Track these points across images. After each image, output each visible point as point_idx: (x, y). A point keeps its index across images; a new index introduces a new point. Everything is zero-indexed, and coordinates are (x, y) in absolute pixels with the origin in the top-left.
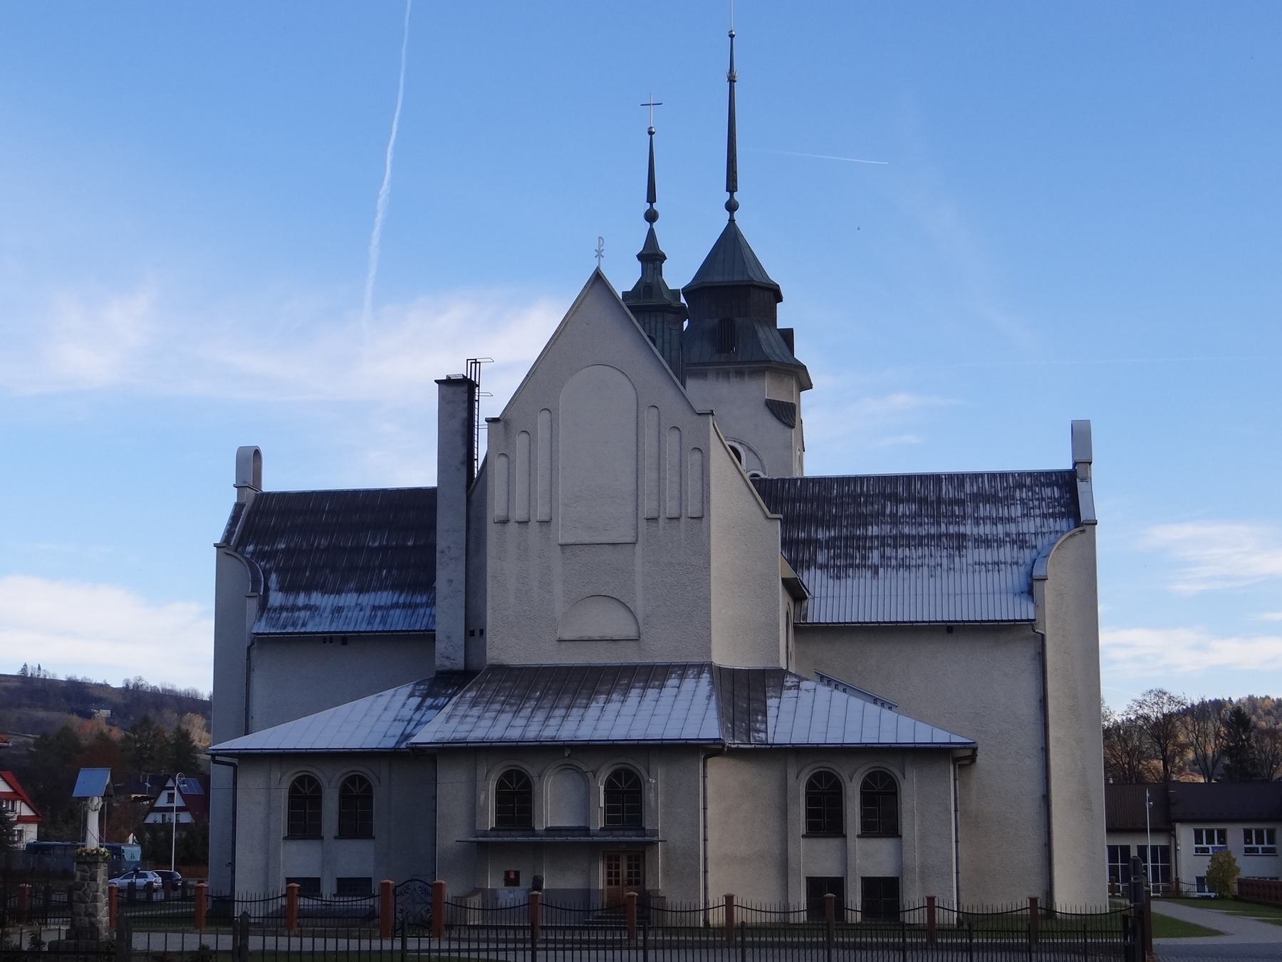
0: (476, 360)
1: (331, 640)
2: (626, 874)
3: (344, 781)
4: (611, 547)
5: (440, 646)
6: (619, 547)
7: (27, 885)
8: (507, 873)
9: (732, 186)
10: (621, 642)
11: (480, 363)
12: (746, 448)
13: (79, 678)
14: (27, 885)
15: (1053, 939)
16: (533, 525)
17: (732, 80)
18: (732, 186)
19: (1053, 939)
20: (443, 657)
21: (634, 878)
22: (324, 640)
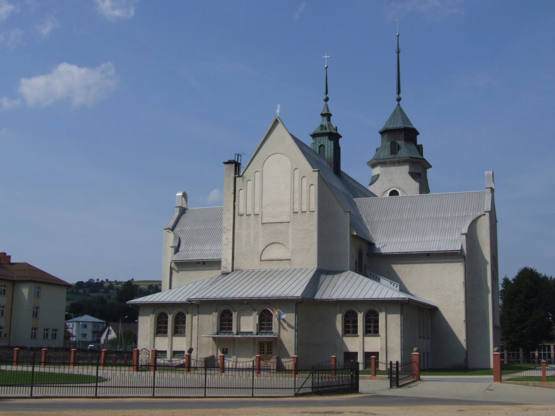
0: (238, 154)
1: (199, 263)
2: (265, 347)
3: (261, 312)
4: (281, 224)
5: (223, 264)
6: (283, 223)
7: (550, 318)
8: (223, 349)
9: (399, 92)
10: (283, 261)
11: (241, 155)
12: (401, 190)
13: (80, 281)
14: (550, 318)
15: (345, 376)
16: (252, 216)
17: (398, 52)
18: (399, 92)
19: (345, 376)
20: (224, 268)
21: (262, 348)
22: (197, 263)
